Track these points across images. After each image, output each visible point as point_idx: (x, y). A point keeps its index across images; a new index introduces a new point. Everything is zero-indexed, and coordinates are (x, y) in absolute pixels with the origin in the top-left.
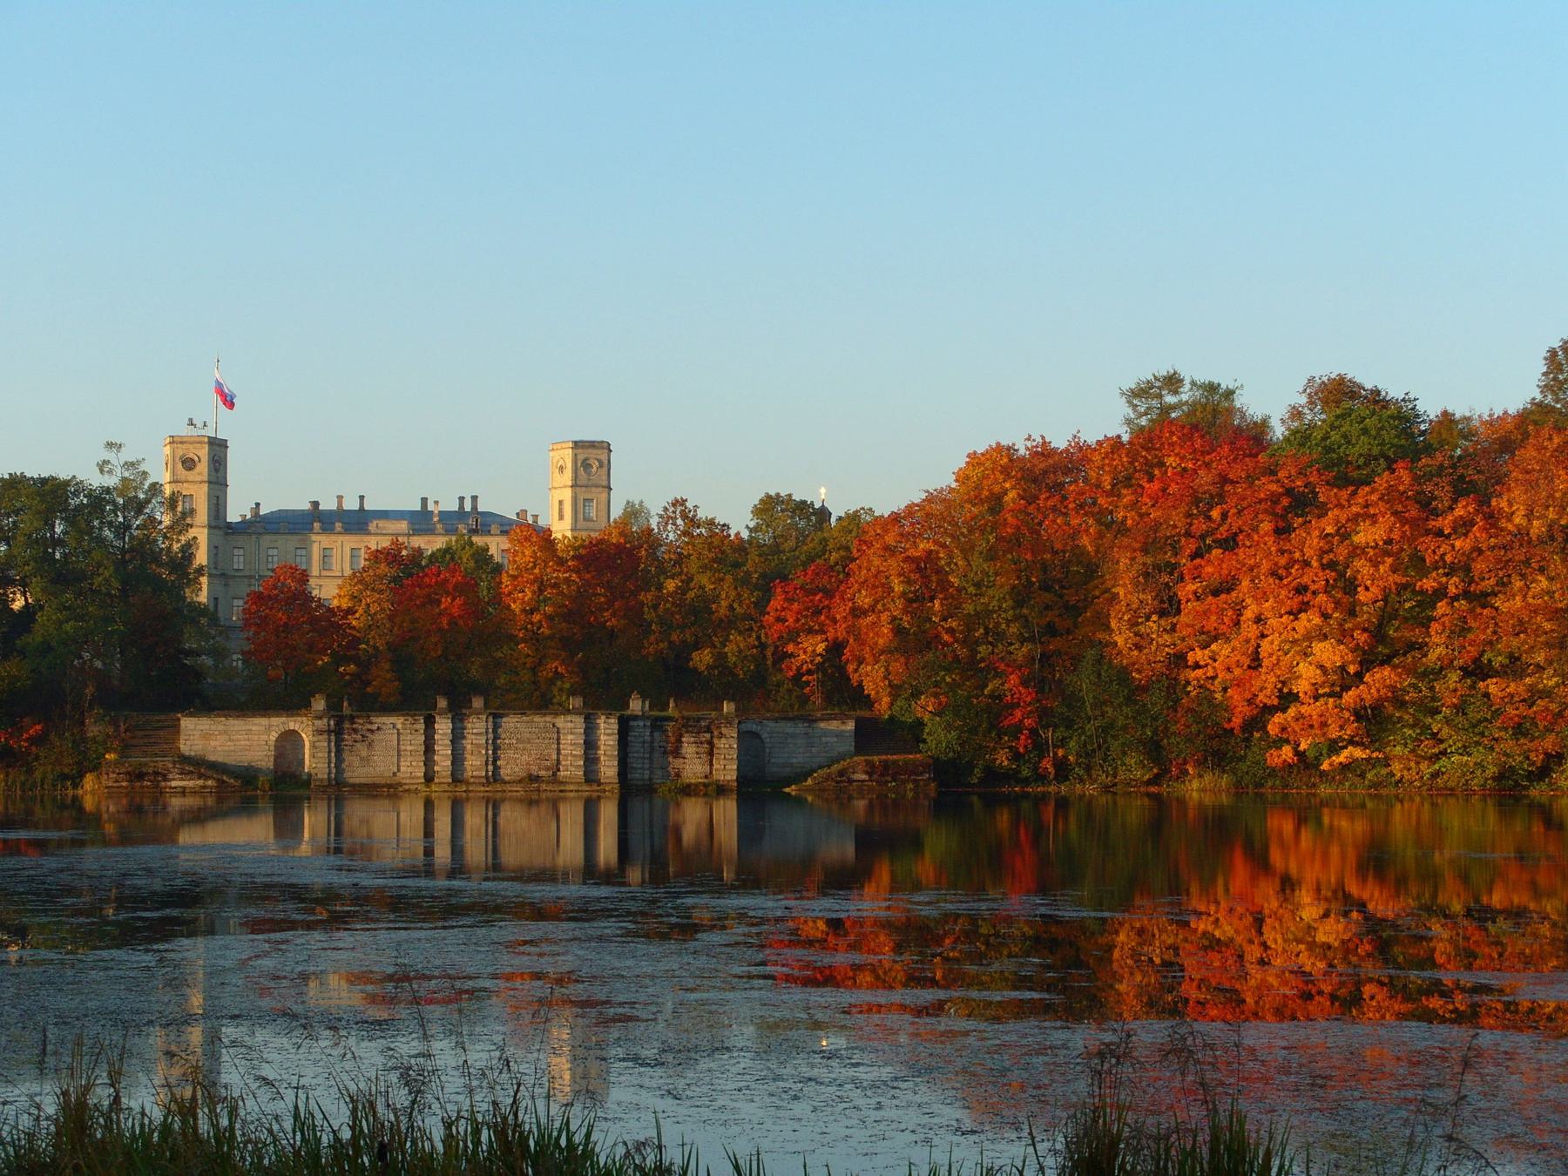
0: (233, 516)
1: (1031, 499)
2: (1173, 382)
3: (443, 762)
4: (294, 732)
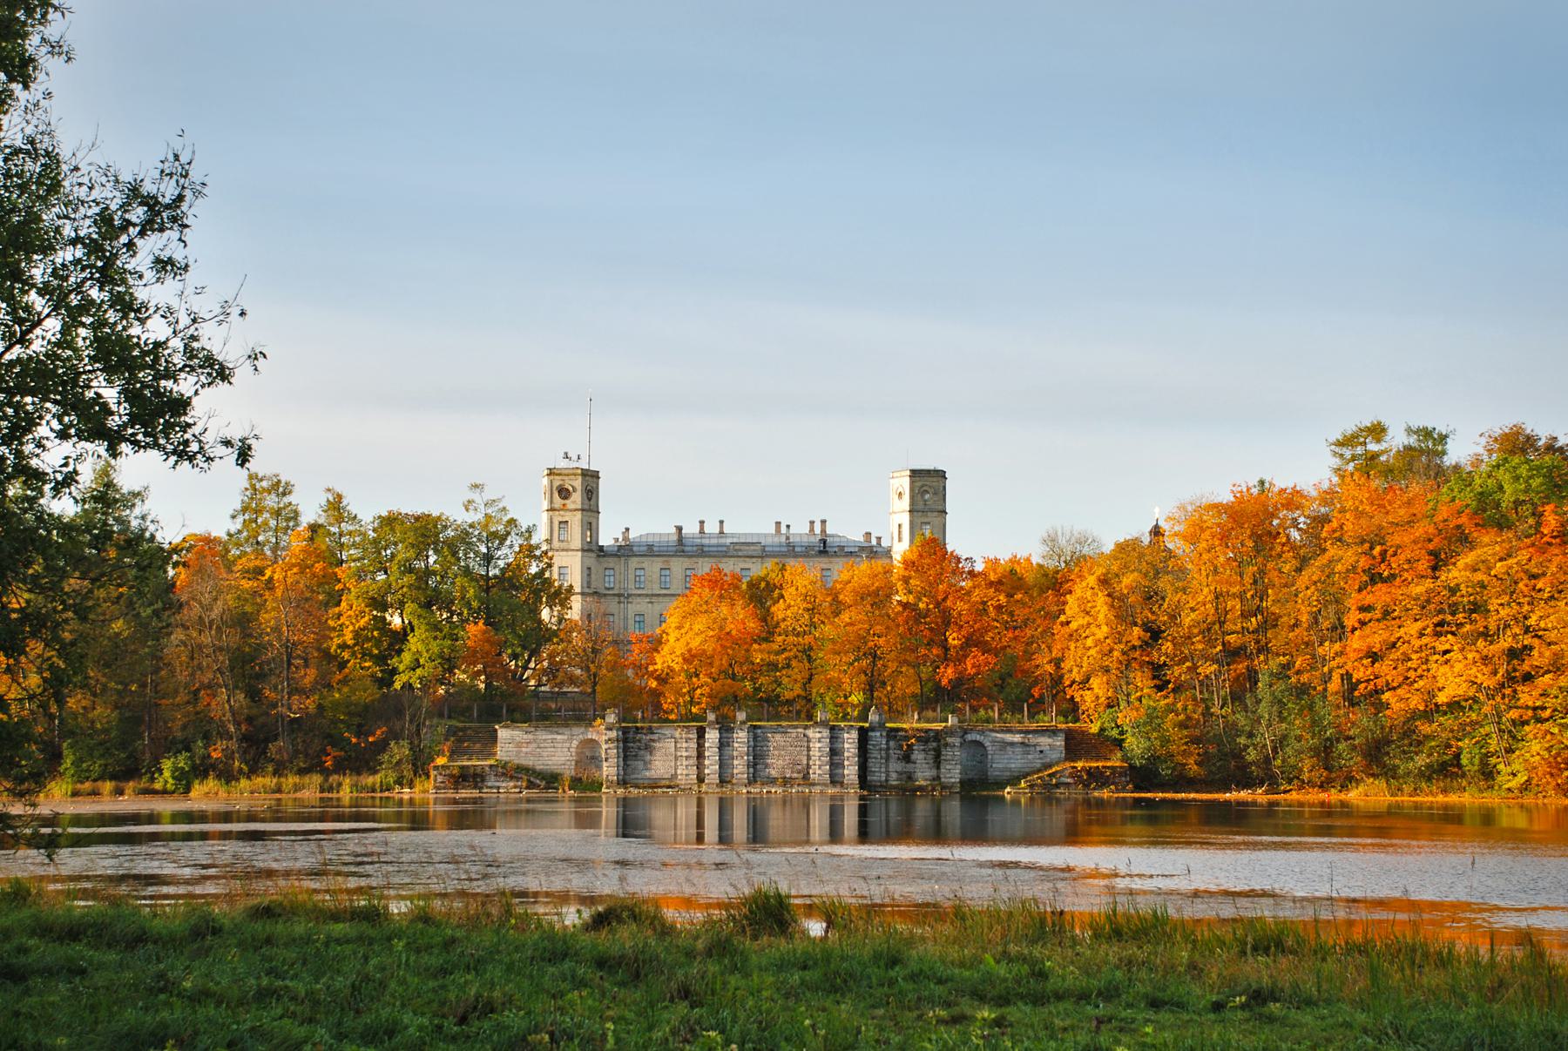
0: (607, 537)
1: (588, 669)
2: (1378, 431)
3: (711, 767)
4: (592, 740)
